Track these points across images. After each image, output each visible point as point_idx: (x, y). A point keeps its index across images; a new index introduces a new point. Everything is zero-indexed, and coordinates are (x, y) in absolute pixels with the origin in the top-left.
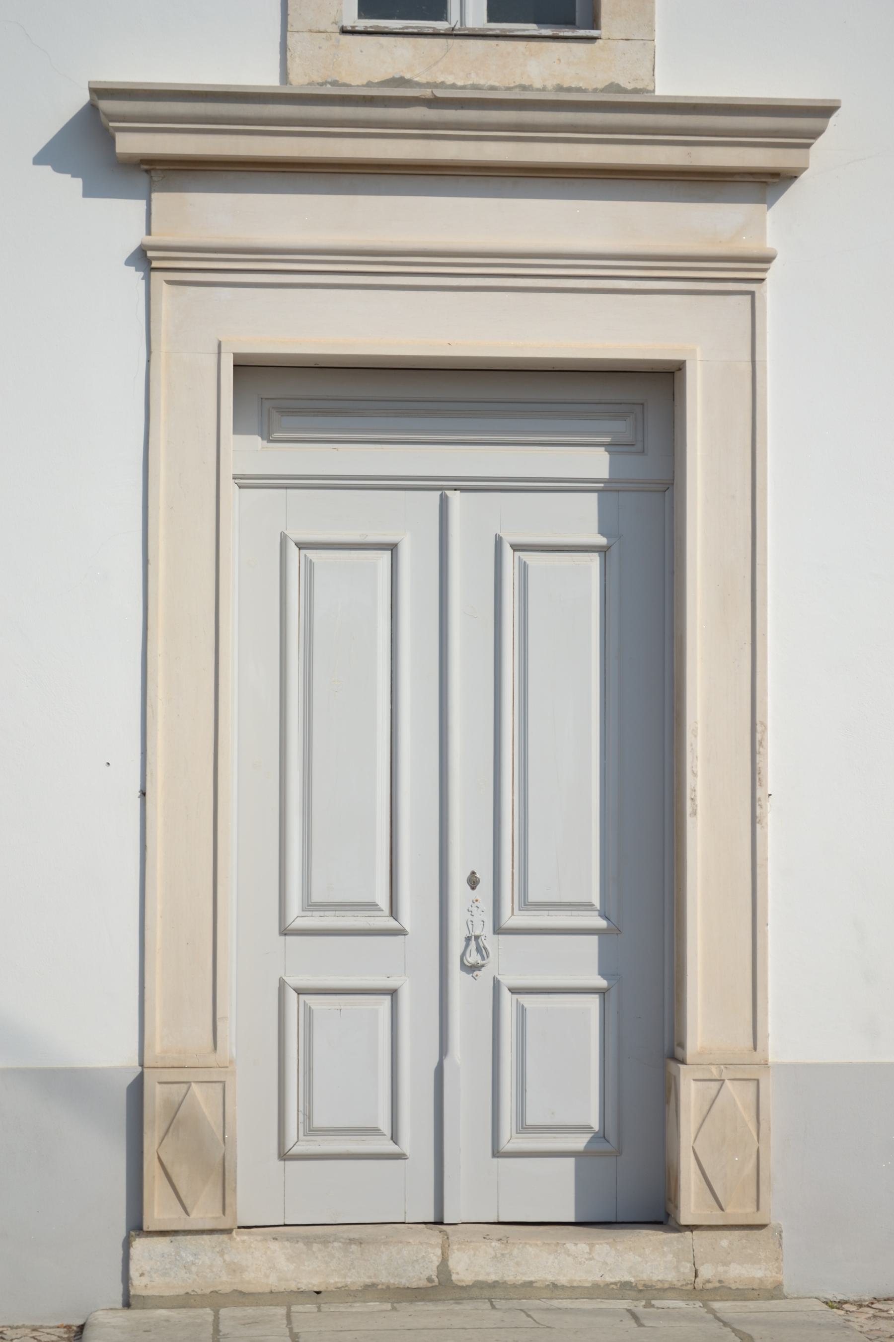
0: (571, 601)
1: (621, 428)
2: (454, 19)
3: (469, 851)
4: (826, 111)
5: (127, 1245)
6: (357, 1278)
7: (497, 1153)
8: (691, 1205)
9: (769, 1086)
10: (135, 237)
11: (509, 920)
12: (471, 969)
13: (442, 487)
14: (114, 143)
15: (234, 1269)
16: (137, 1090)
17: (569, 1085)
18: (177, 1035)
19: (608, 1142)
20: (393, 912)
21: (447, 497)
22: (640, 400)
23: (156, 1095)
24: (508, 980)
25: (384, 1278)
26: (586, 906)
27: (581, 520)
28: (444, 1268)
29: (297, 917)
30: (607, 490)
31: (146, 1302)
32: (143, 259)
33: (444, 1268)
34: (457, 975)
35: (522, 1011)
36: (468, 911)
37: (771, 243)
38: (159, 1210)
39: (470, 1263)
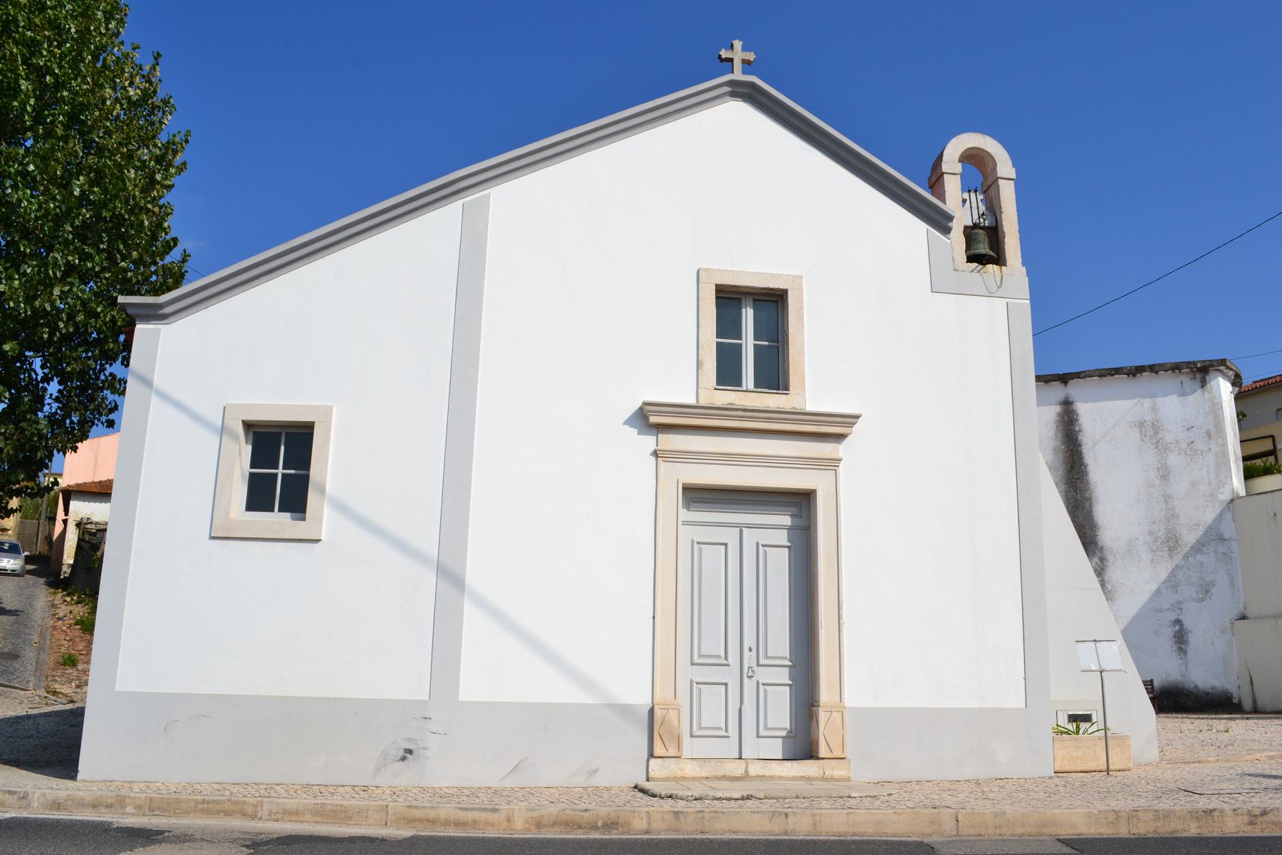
0: (779, 563)
1: (794, 510)
2: (744, 388)
3: (749, 641)
4: (858, 417)
5: (648, 761)
6: (720, 773)
7: (758, 736)
8: (823, 752)
9: (846, 713)
10: (653, 447)
11: (762, 662)
12: (750, 677)
13: (741, 527)
14: (648, 419)
15: (681, 769)
16: (652, 711)
17: (780, 714)
18: (664, 694)
19: (1108, 594)
20: (726, 658)
21: (991, 248)
22: (800, 503)
23: (658, 713)
24: (761, 681)
25: (728, 774)
26: (785, 658)
27: (782, 537)
28: (746, 770)
29: (696, 660)
30: (790, 529)
31: (654, 780)
32: (655, 454)
33: (746, 770)
34: (746, 680)
35: (766, 691)
36: (749, 658)
37: (841, 455)
38: (659, 750)
39: (755, 769)
